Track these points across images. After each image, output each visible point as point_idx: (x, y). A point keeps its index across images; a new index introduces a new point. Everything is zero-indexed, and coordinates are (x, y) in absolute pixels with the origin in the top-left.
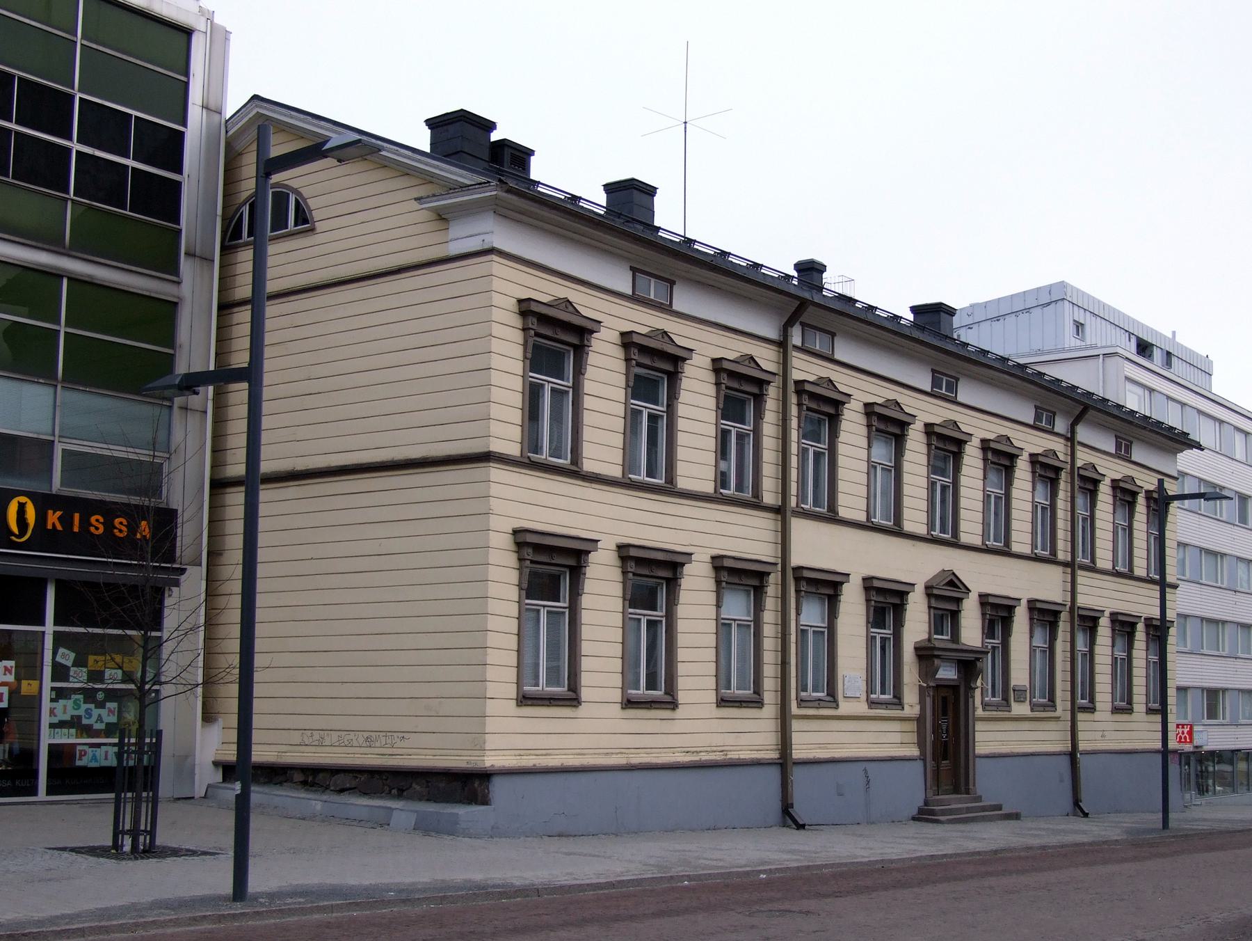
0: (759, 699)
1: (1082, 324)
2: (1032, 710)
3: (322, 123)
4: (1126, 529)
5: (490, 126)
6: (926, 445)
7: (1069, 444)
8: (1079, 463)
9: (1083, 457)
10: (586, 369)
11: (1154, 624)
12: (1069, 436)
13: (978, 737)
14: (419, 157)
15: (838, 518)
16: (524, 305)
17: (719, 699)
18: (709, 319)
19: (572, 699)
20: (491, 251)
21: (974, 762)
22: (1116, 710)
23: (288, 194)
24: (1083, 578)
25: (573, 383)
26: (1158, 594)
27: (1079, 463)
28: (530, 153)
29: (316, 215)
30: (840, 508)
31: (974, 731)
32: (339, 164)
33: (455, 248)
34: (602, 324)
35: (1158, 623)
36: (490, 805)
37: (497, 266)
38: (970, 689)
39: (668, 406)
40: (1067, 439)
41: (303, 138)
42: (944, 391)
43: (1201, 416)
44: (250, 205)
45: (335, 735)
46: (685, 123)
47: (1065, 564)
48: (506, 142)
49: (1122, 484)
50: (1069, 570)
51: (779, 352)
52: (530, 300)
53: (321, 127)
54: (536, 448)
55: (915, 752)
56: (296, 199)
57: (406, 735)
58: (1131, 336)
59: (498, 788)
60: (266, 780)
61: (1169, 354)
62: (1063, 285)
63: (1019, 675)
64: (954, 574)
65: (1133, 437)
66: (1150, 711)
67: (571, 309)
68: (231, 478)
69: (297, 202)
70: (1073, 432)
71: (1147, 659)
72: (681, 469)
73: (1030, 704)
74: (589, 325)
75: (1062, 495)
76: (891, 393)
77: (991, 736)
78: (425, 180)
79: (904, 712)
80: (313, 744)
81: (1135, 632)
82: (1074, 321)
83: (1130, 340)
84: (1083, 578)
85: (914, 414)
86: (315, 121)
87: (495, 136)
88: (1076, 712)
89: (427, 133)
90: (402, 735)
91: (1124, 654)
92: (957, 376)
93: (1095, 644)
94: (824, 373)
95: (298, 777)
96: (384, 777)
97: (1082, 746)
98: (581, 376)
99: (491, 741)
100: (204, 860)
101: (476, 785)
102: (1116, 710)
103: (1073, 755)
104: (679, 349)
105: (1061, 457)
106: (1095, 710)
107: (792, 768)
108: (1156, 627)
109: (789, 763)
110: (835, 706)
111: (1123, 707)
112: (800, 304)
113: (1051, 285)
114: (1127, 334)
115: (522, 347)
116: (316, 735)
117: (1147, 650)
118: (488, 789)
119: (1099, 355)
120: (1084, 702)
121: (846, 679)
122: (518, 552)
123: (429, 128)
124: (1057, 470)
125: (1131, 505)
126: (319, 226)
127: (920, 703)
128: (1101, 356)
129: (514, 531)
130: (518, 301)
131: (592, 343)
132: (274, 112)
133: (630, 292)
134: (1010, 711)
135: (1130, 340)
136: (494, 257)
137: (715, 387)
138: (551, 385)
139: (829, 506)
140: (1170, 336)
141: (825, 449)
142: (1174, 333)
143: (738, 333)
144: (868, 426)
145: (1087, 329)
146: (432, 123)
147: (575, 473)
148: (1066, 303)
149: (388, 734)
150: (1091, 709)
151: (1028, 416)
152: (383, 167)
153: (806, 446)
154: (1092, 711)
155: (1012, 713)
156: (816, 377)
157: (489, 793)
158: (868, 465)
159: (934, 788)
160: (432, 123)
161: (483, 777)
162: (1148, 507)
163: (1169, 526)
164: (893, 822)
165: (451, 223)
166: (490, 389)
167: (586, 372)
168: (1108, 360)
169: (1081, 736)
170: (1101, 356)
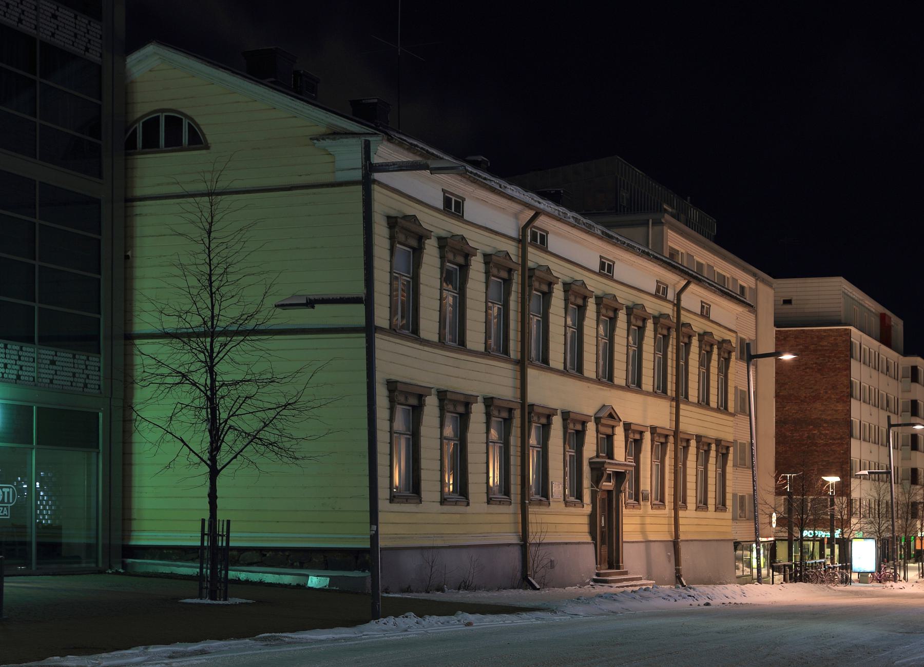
0: (509, 499)
12: (676, 303)
21: (622, 545)
31: (622, 524)
32: (676, 293)
40: (674, 305)
42: (606, 272)
44: (143, 123)
47: (673, 400)
50: (674, 404)
51: (518, 247)
56: (189, 124)
60: (178, 557)
63: (647, 483)
64: (613, 408)
68: (137, 334)
70: (679, 299)
71: (696, 468)
91: (702, 467)
92: (710, 303)
94: (409, 211)
97: (682, 537)
102: (697, 508)
105: (514, 258)
111: (8, 493)
112: (535, 213)
120: (680, 502)
150: (685, 507)
154: (684, 509)
169: (682, 528)
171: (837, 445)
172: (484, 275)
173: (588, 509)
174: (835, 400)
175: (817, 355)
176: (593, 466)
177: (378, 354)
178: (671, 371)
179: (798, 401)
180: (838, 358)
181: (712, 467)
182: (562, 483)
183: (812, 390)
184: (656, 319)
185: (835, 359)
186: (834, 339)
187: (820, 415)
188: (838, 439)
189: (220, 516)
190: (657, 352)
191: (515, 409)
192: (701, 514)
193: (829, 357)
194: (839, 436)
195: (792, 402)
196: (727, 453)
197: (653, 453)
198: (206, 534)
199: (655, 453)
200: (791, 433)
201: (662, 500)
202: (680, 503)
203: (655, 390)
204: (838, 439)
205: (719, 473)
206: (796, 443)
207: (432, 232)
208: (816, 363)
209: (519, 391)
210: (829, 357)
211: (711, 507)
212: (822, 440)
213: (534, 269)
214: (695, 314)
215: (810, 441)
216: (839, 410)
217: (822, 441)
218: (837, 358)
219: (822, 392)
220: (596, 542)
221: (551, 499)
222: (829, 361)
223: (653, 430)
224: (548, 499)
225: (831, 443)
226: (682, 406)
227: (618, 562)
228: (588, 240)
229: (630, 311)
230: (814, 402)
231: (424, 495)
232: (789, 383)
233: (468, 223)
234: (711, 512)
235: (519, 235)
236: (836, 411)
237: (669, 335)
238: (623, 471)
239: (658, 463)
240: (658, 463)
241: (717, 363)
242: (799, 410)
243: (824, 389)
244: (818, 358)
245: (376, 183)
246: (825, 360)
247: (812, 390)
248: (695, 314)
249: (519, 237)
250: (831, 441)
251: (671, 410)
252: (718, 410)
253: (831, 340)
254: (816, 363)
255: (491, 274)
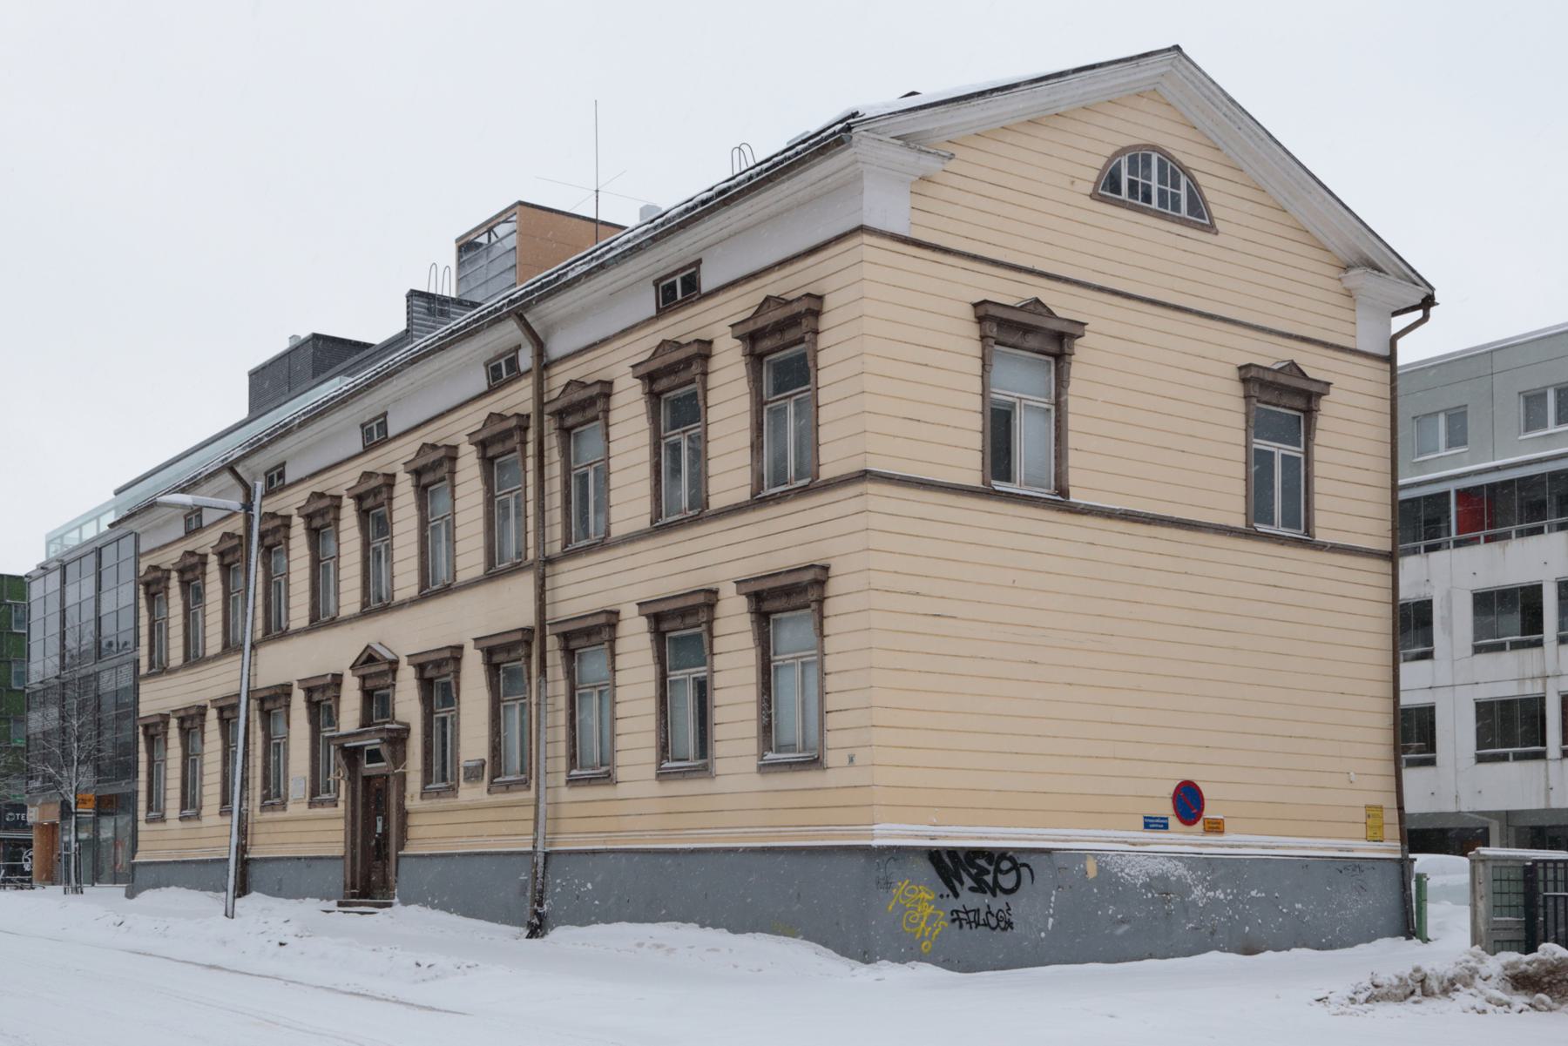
10: (1069, 382)
18: (938, 243)
30: (1316, 529)
34: (1086, 327)
52: (985, 302)
54: (1004, 473)
67: (1041, 309)
72: (1319, 519)
74: (1315, 388)
95: (386, 828)
98: (1063, 389)
100: (677, 928)
107: (345, 852)
131: (1075, 350)
136: (866, 239)
137: (1243, 400)
138: (1281, 452)
141: (1300, 452)
144: (1245, 397)
147: (1308, 543)
153: (1010, 399)
164: (424, 980)
167: (1069, 385)
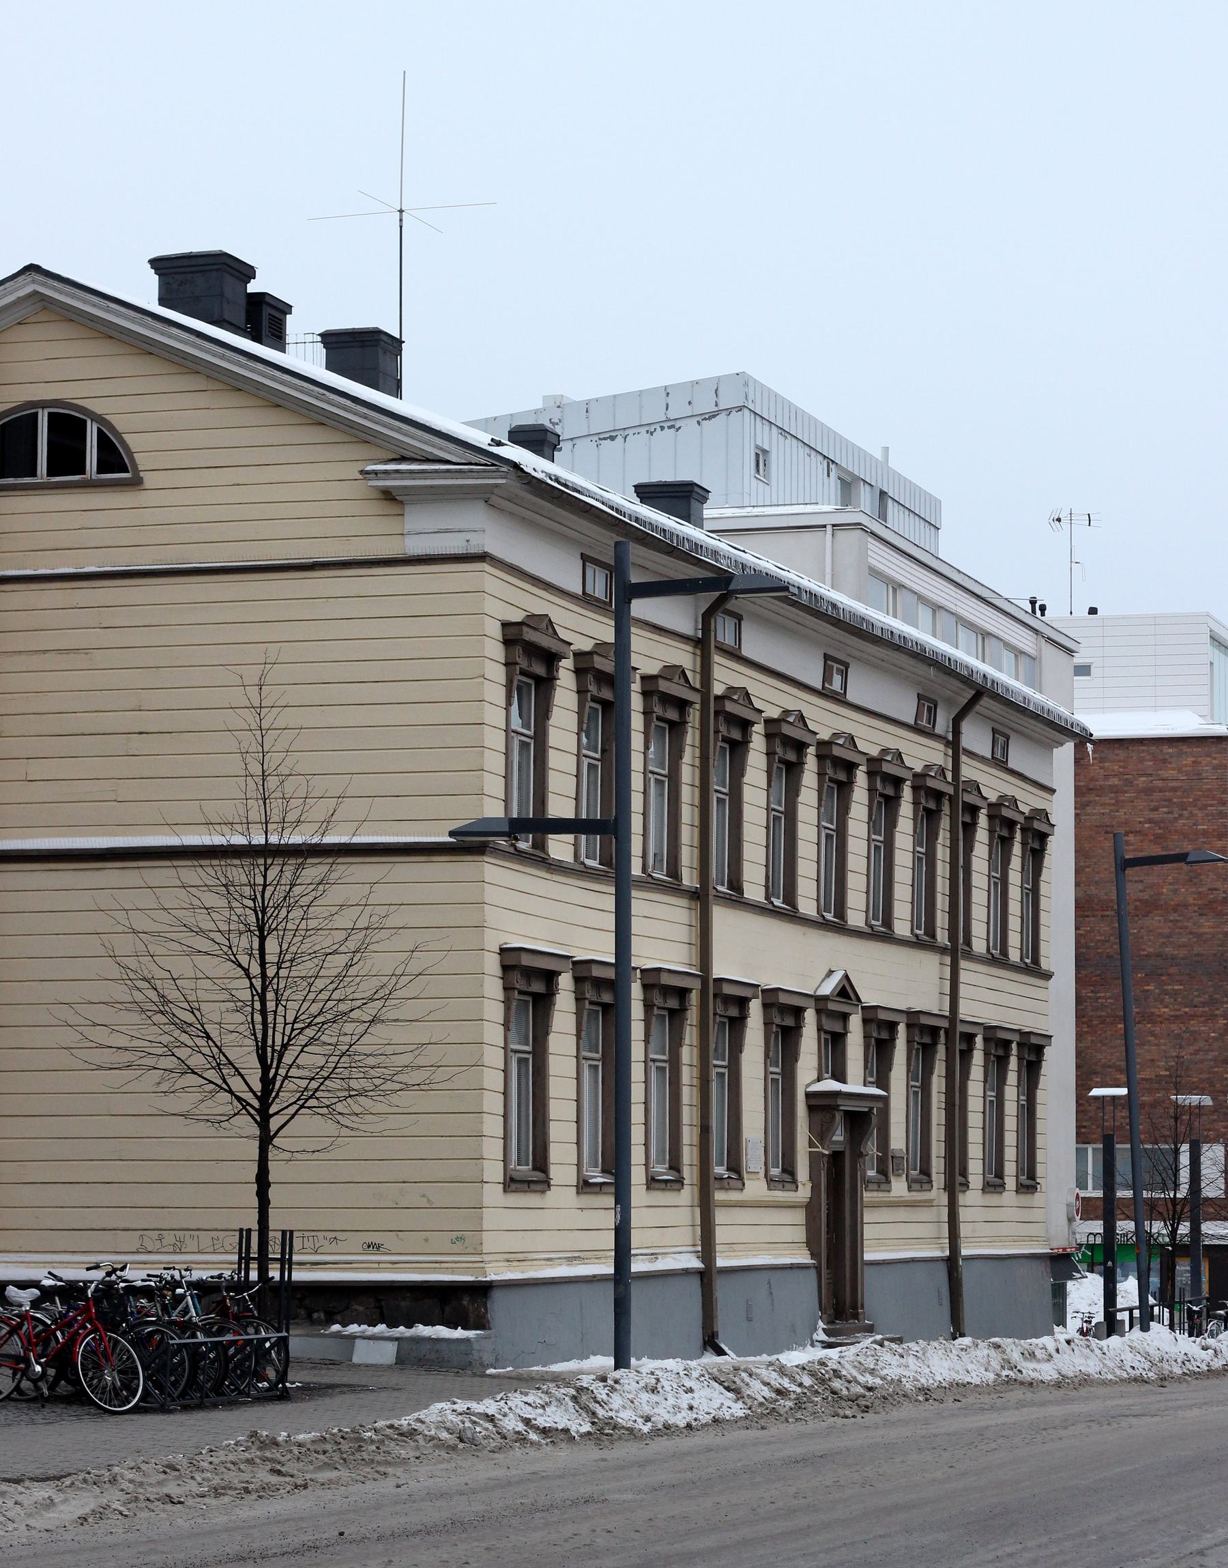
1: (765, 452)
2: (910, 1189)
3: (175, 331)
4: (663, 782)
5: (248, 272)
6: (987, 832)
7: (950, 752)
8: (718, 689)
9: (725, 676)
11: (524, 963)
13: (869, 1232)
14: (365, 411)
15: (743, 900)
16: (513, 630)
17: (508, 1178)
19: (546, 1184)
20: (483, 557)
21: (862, 1270)
22: (511, 1183)
23: (85, 422)
24: (723, 919)
25: (535, 731)
26: (610, 903)
27: (718, 689)
28: (286, 309)
29: (142, 461)
31: (862, 1223)
33: (416, 546)
35: (610, 974)
36: (490, 1329)
37: (488, 578)
38: (858, 1155)
39: (603, 751)
40: (948, 744)
41: (240, 390)
43: (960, 627)
45: (206, 1239)
46: (401, 211)
47: (943, 950)
48: (267, 299)
49: (664, 686)
50: (948, 960)
53: (170, 336)
55: (804, 1258)
57: (339, 1235)
58: (832, 466)
59: (499, 1307)
61: (883, 494)
62: (743, 379)
65: (1013, 730)
66: (584, 1186)
69: (101, 435)
70: (957, 732)
73: (907, 1180)
75: (689, 756)
76: (538, 603)
77: (745, 1234)
78: (356, 436)
79: (493, 1193)
80: (163, 1250)
81: (972, 1050)
82: (757, 447)
83: (829, 476)
84: (723, 919)
85: (816, 731)
86: (159, 325)
87: (253, 287)
88: (957, 1190)
89: (154, 279)
90: (333, 1235)
91: (917, 1084)
92: (848, 660)
93: (1037, 1088)
94: (538, 607)
96: (299, 1296)
99: (490, 1243)
101: (465, 1303)
102: (511, 1183)
103: (952, 1262)
104: (560, 643)
106: (968, 1187)
108: (599, 983)
109: (714, 1271)
110: (794, 1188)
113: (719, 378)
114: (825, 463)
115: (643, 735)
116: (169, 1238)
117: (985, 1081)
118: (486, 1309)
119: (825, 526)
121: (750, 1144)
122: (502, 978)
123: (156, 273)
124: (682, 705)
125: (545, 685)
126: (149, 479)
127: (811, 1179)
128: (829, 528)
129: (501, 950)
130: (502, 624)
132: (73, 297)
133: (912, 722)
134: (889, 1191)
135: (829, 476)
136: (486, 566)
139: (730, 882)
140: (878, 455)
142: (886, 450)
143: (662, 633)
145: (773, 458)
146: (160, 265)
148: (746, 412)
149: (306, 1234)
151: (906, 709)
152: (273, 406)
154: (539, 1187)
155: (893, 1194)
156: (661, 664)
157: (487, 1312)
158: (913, 857)
159: (828, 1312)
160: (160, 265)
161: (482, 1290)
162: (581, 692)
163: (1044, 876)
165: (407, 508)
166: (483, 753)
168: (840, 534)
170: (829, 528)
171: (1202, 1019)
172: (575, 696)
173: (804, 1192)
174: (1196, 908)
175: (1152, 801)
176: (814, 1102)
177: (637, 925)
178: (942, 886)
179: (1107, 913)
180: (1204, 808)
181: (1011, 1092)
182: (763, 1141)
183: (1140, 886)
184: (919, 780)
185: (1196, 811)
186: (1193, 762)
187: (1160, 947)
188: (1204, 1004)
189: (277, 1222)
190: (585, 752)
191: (559, 973)
192: (993, 1199)
193: (1183, 807)
194: (1207, 996)
195: (1094, 916)
196: (892, 1040)
197: (583, 1034)
198: (254, 1259)
199: (588, 1034)
200: (1092, 992)
201: (926, 1172)
202: (720, 1170)
203: (582, 858)
204: (1204, 1004)
205: (990, 1101)
206: (1104, 1014)
207: (638, 669)
208: (1150, 821)
209: (695, 951)
210: (1183, 807)
211: (1010, 1183)
212: (1166, 1007)
213: (589, 654)
214: (982, 759)
215: (1137, 1010)
216: (1206, 933)
217: (1166, 1010)
218: (1199, 809)
219: (1165, 890)
220: (820, 1263)
221: (745, 1176)
222: (1181, 816)
223: (913, 1017)
224: (741, 1178)
225: (1186, 1013)
226: (963, 964)
227: (854, 1306)
228: (773, 614)
229: (773, 729)
230: (1146, 915)
231: (555, 1172)
232: (1087, 870)
233: (970, 755)
234: (1009, 1196)
235: (696, 629)
236: (1199, 936)
237: (939, 811)
238: (867, 1110)
239: (917, 1089)
240: (917, 1089)
241: (815, 794)
242: (1111, 935)
243: (1170, 884)
244: (1156, 809)
245: (488, 558)
246: (1172, 813)
247: (1140, 886)
248: (982, 759)
249: (696, 633)
250: (1187, 1010)
251: (941, 972)
252: (870, 935)
253: (1186, 765)
254: (1150, 821)
255: (654, 715)
